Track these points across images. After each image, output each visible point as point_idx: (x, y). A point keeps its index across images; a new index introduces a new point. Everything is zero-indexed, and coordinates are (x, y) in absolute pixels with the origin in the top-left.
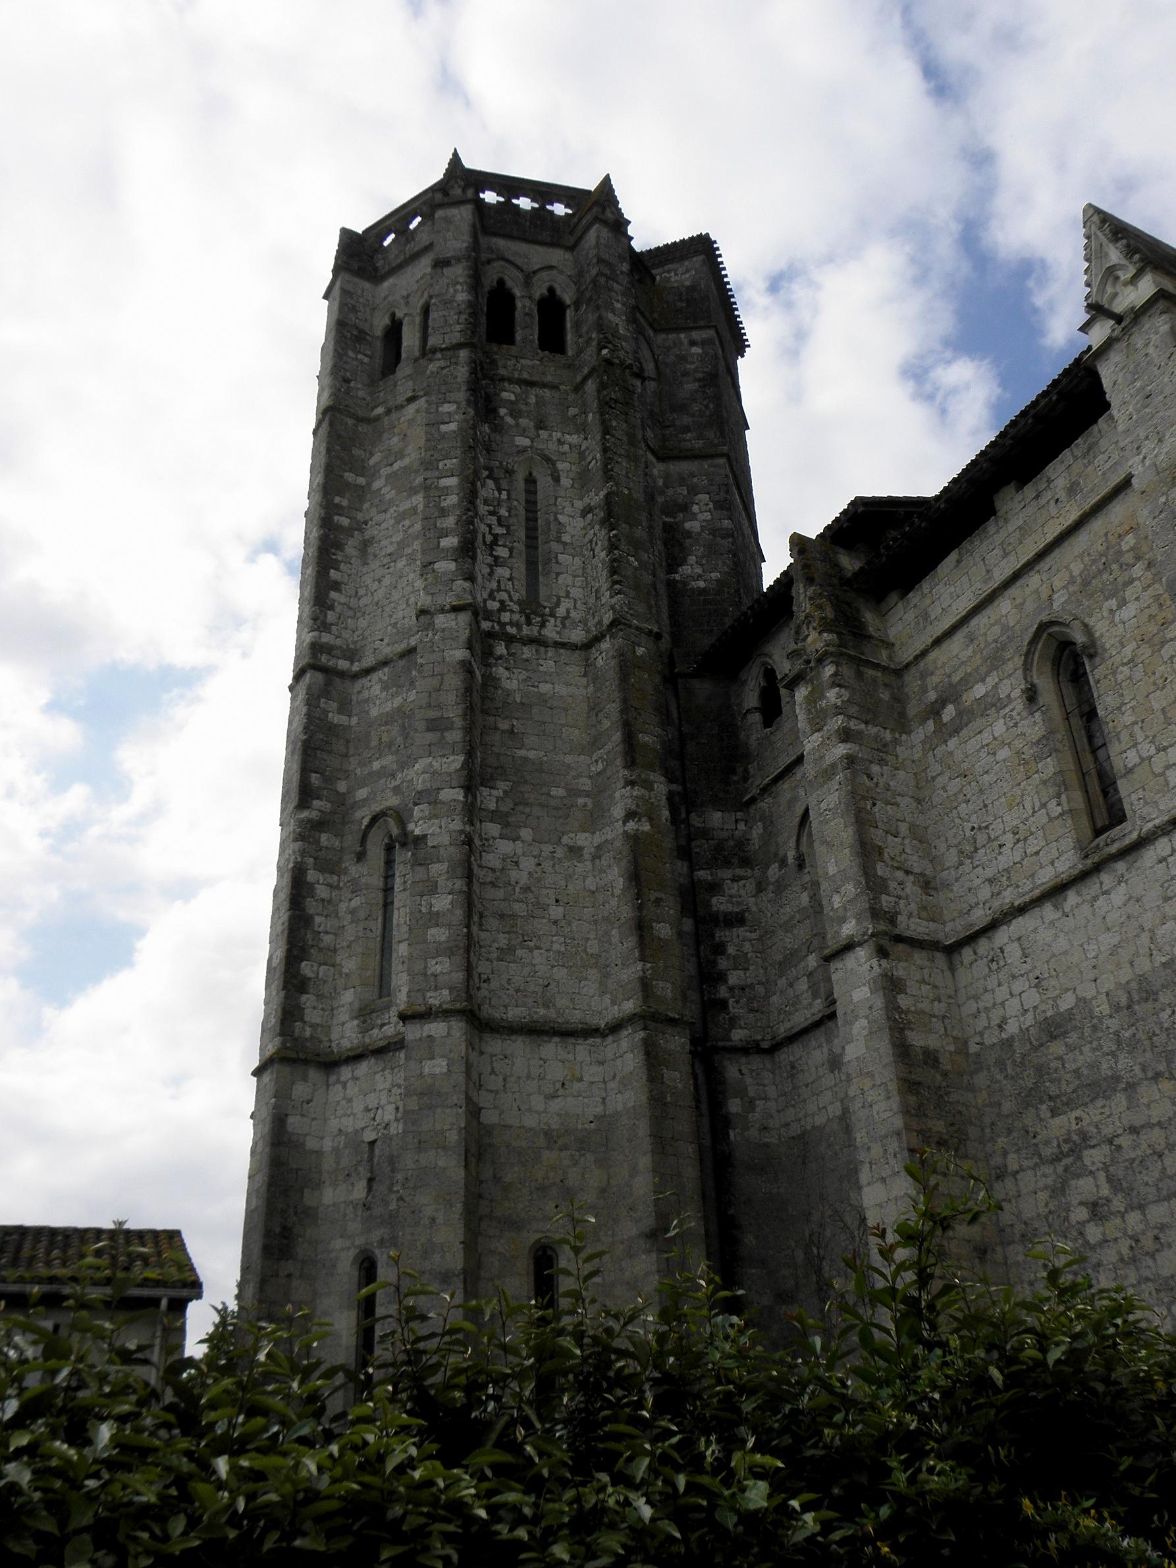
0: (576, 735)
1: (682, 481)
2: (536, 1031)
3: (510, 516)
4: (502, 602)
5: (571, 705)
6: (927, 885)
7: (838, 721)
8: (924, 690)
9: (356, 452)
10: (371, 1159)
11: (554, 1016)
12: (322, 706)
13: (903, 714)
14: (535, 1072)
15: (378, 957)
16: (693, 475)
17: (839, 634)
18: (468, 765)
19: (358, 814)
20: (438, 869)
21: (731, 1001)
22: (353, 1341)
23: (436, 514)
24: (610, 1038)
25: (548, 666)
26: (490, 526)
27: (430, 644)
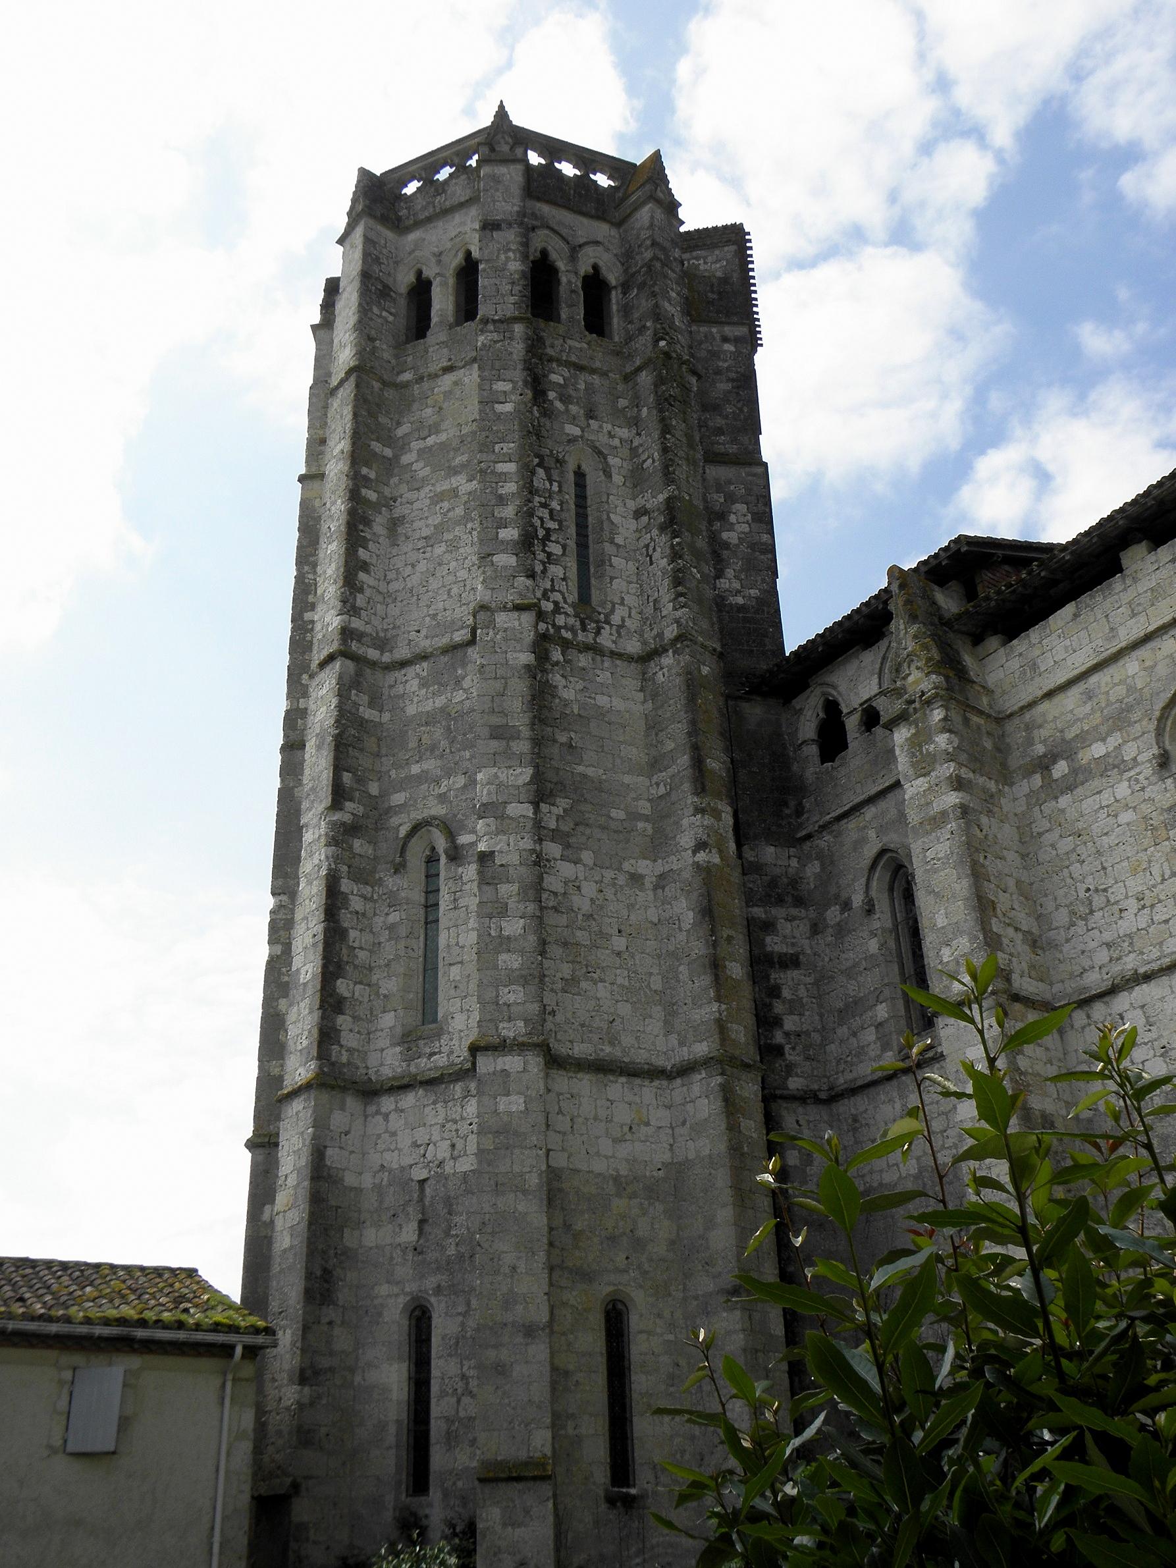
0: (636, 753)
1: (719, 488)
2: (602, 1068)
3: (562, 510)
4: (556, 603)
5: (638, 722)
6: (1034, 943)
7: (949, 769)
8: (1030, 742)
9: (383, 420)
10: (421, 1199)
11: (619, 1054)
12: (353, 698)
13: (1004, 765)
14: (602, 1113)
15: (421, 979)
16: (730, 482)
17: (947, 678)
18: (538, 777)
19: (394, 821)
20: (508, 890)
21: (787, 1048)
22: (404, 1396)
23: (493, 503)
24: (679, 1081)
25: (604, 677)
26: (541, 519)
27: (491, 644)
